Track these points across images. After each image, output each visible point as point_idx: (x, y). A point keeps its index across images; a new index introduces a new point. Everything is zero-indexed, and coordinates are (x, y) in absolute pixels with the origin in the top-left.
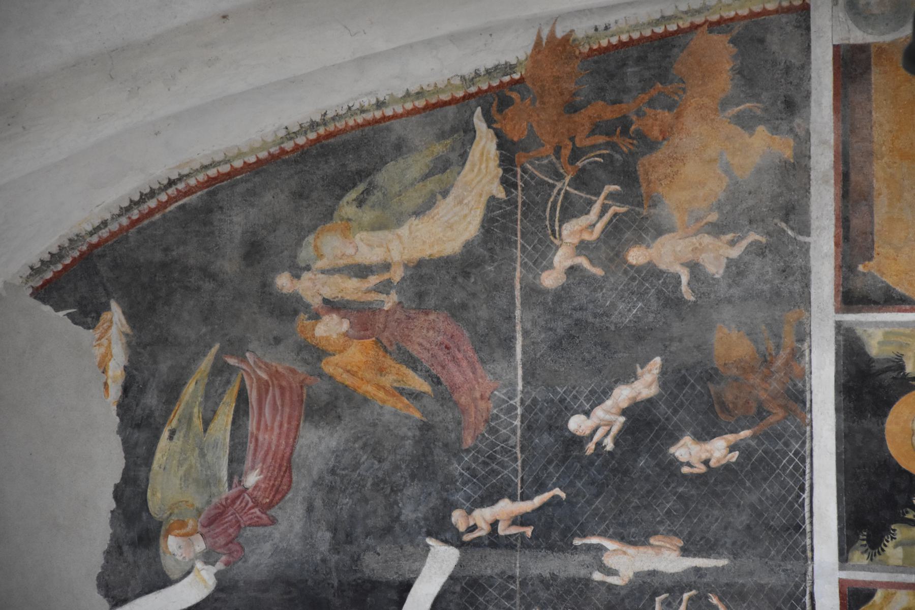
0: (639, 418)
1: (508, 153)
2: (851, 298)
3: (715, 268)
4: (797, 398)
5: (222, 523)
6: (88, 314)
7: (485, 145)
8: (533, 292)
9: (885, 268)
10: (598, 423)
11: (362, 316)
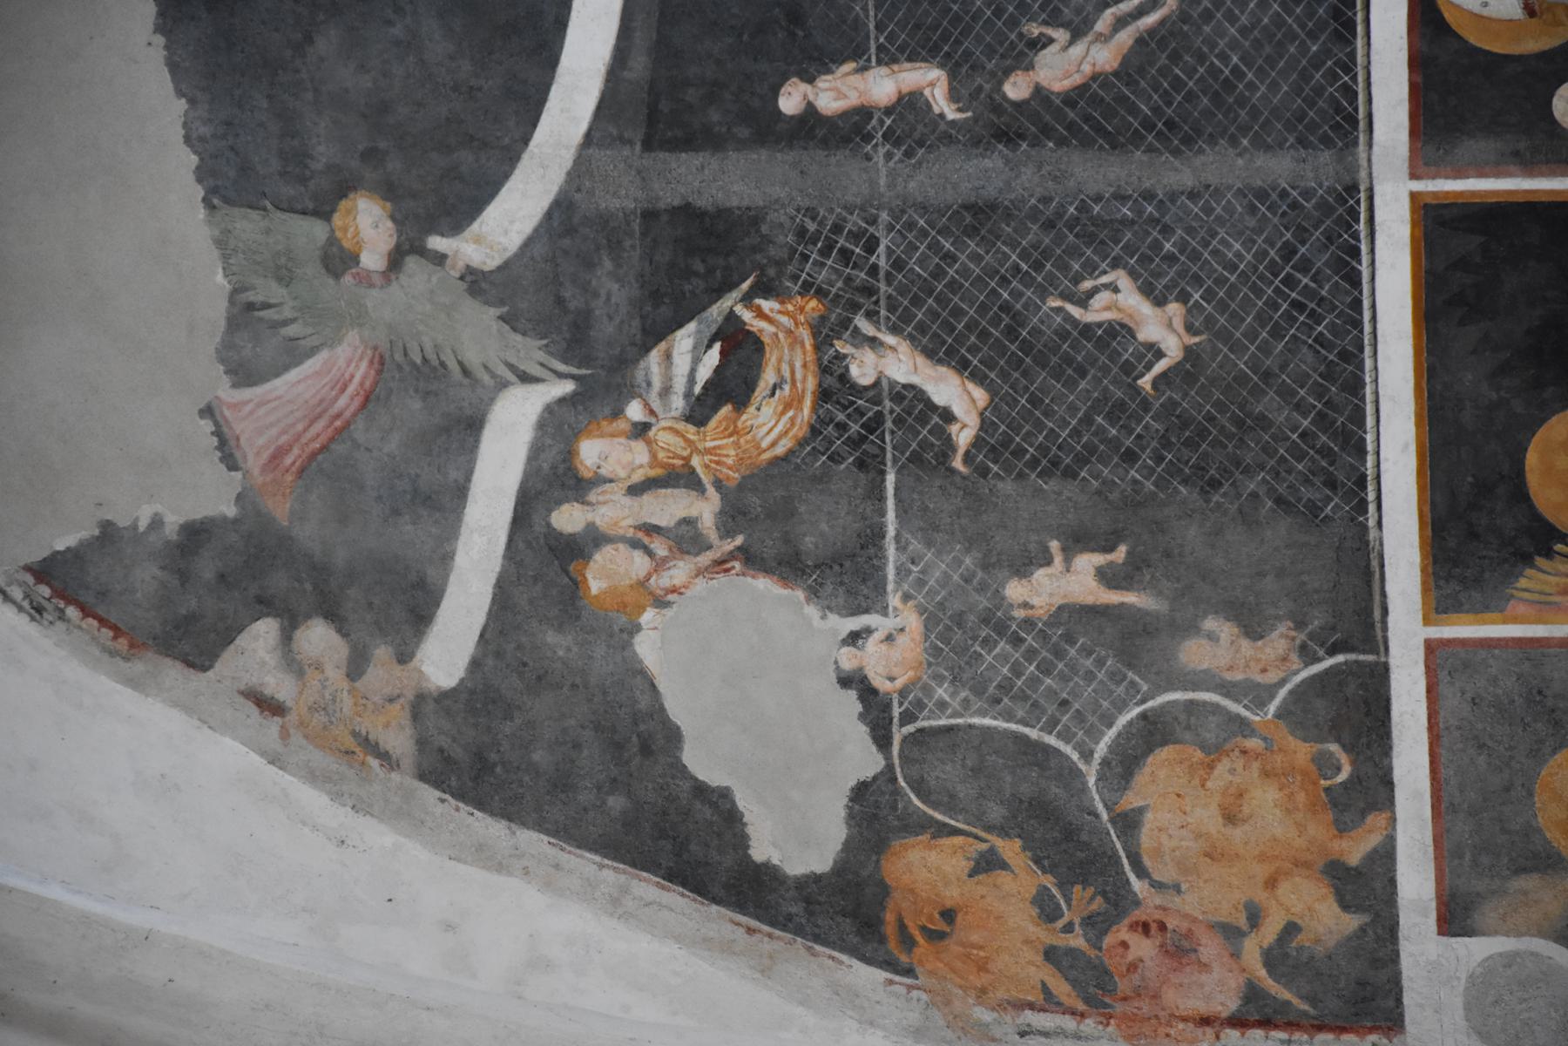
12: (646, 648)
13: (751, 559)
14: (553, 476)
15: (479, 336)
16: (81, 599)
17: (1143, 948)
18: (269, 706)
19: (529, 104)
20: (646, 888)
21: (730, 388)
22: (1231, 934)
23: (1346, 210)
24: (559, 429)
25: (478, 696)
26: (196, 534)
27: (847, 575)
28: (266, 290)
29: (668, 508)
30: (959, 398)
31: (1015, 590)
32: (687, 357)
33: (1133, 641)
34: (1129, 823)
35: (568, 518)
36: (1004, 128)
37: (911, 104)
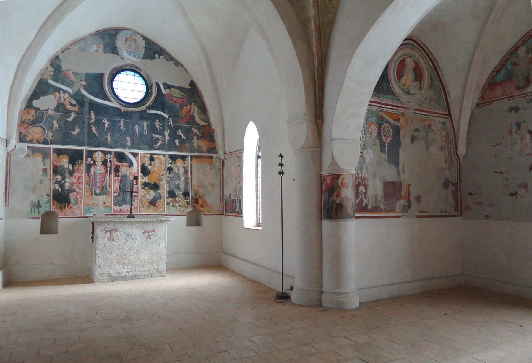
0: (180, 136)
1: (204, 126)
2: (191, 157)
3: (194, 144)
4: (182, 151)
5: (170, 95)
6: (190, 85)
7: (205, 124)
8: (192, 127)
9: (194, 159)
10: (180, 132)
11: (189, 111)
12: (51, 96)
13: (58, 104)
14: (65, 92)
15: (76, 89)
16: (502, 70)
17: (26, 126)
18: (47, 69)
19: (92, 95)
20: (31, 92)
21: (71, 104)
22: (27, 132)
23: (83, 145)
24: (69, 93)
25: (47, 84)
26: (61, 67)
27: (57, 109)
28: (79, 75)
29: (62, 99)
30: (70, 119)
31: (55, 121)
32: (74, 102)
33: (51, 128)
34: (36, 126)
35: (61, 92)
36: (90, 125)
37: (92, 119)
